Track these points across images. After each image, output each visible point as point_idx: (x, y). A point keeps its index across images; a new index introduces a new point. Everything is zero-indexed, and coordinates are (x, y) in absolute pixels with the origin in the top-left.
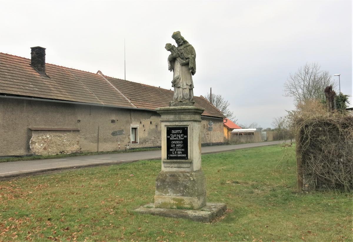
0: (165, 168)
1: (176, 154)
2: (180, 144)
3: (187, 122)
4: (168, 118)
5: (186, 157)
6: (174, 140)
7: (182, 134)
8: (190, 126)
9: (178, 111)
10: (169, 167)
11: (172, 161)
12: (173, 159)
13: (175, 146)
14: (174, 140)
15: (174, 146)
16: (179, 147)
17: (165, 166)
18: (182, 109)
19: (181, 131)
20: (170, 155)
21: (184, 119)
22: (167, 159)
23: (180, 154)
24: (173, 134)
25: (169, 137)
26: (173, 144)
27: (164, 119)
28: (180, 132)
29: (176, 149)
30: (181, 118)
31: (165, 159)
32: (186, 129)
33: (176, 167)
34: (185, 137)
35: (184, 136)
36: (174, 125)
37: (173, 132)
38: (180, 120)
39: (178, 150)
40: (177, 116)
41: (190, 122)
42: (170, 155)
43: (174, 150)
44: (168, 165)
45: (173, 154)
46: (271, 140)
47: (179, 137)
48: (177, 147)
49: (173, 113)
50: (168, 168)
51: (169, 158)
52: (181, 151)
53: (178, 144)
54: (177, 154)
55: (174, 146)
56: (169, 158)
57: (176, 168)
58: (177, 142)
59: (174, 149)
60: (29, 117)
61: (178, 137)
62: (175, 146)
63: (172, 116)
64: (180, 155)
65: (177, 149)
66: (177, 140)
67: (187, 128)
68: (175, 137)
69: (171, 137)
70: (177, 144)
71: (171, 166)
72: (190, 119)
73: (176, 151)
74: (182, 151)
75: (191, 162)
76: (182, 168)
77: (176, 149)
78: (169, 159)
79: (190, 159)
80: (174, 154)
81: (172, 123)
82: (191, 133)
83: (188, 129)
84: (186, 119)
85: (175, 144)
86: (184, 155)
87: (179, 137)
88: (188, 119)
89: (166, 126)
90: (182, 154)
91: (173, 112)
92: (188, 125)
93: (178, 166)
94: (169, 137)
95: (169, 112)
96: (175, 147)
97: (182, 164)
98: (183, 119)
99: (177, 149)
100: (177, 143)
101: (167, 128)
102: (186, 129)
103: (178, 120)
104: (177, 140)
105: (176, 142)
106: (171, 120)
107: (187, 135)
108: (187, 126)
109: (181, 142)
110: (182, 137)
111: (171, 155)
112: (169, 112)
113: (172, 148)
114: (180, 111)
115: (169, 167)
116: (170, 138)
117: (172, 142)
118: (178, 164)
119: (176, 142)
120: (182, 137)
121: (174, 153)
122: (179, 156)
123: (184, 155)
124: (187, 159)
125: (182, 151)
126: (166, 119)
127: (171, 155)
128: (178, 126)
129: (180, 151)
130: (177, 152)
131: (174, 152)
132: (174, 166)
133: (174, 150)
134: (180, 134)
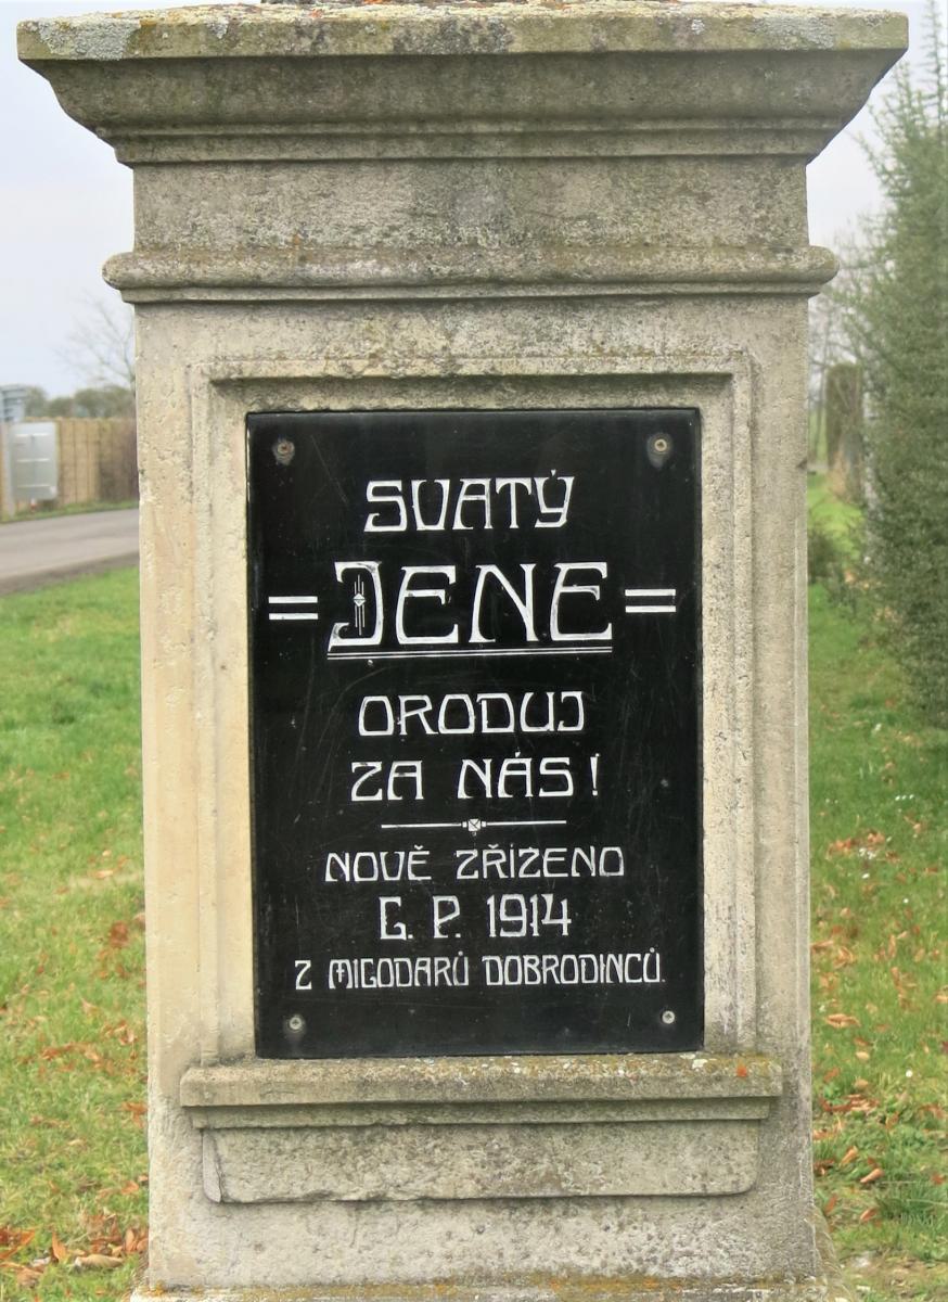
0: (234, 1228)
1: (448, 949)
2: (537, 747)
3: (682, 312)
4: (283, 232)
5: (655, 999)
6: (401, 677)
7: (571, 543)
8: (755, 390)
9: (522, 96)
10: (315, 1200)
11: (385, 1074)
12: (380, 1050)
13: (441, 781)
14: (401, 677)
15: (405, 786)
16: (518, 804)
17: (236, 1191)
18: (634, 44)
19: (554, 494)
20: (318, 975)
21: (644, 264)
22: (270, 1042)
23: (547, 942)
24: (395, 553)
25: (295, 607)
26: (388, 750)
27: (196, 255)
28: (527, 501)
29: (443, 847)
30: (551, 243)
31: (226, 1059)
32: (660, 446)
33: (457, 1203)
34: (650, 601)
35: (612, 588)
36: (418, 368)
37: (388, 514)
38: (559, 279)
39: (495, 859)
40: (485, 193)
41: (761, 309)
42: (318, 975)
43: (411, 859)
44: (300, 1170)
45: (394, 949)
46: (83, 496)
47: (527, 613)
48: (479, 804)
49: (392, 126)
50: (285, 1228)
51: (296, 1024)
52: (560, 889)
53: (493, 750)
54: (471, 936)
55: (405, 786)
56: (296, 1024)
57: (461, 1225)
58: (478, 709)
59: (405, 841)
60: (934, 446)
61: (502, 623)
62: (441, 781)
63: (368, 179)
64: (532, 969)
65: (467, 840)
66: (478, 676)
67: (685, 430)
68: (423, 618)
69: (347, 612)
70: (480, 747)
71: (367, 1185)
72: (754, 262)
73: (445, 882)
74: (580, 892)
75: (773, 1101)
76: (579, 1223)
77: (443, 847)
78: (316, 1045)
79: (745, 1037)
80: (423, 945)
81: (380, 324)
82: (768, 529)
83: (712, 448)
84: (687, 263)
85: (441, 757)
86: (613, 967)
87: (527, 613)
88: (715, 263)
89: (228, 386)
90: (575, 944)
91: (414, 97)
92: (723, 380)
93: (507, 1180)
94: (295, 607)
95: (333, 97)
96: (440, 799)
97: (592, 1142)
98: (615, 246)
99: (467, 840)
100: (479, 723)
101: (262, 436)
102: (660, 446)
103: (510, 265)
104: (478, 676)
105: (457, 715)
106: (362, 268)
107: (682, 568)
108: (688, 399)
109: (566, 712)
110: (578, 615)
111: (347, 972)
112: (333, 97)
113: (362, 830)
114: (562, 93)
115: (315, 1200)
116: (321, 630)
117: (376, 717)
118: (501, 1139)
119: (457, 715)
120: (578, 615)
121: (421, 924)
122: (503, 972)
123: (613, 967)
124: (690, 1033)
125: (580, 892)
126: (253, 249)
127: (347, 972)
128: (489, 402)
129: (529, 888)
130: (473, 897)
131: (415, 909)
132: (420, 1187)
133: (411, 859)
134: (547, 550)
